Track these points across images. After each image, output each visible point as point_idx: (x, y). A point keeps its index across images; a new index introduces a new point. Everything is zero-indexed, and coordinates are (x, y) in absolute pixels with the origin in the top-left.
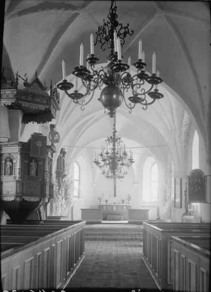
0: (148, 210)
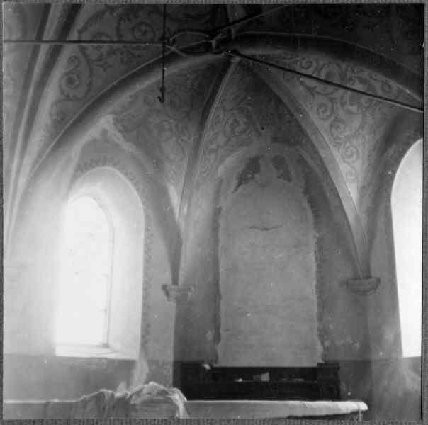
0: (420, 8)
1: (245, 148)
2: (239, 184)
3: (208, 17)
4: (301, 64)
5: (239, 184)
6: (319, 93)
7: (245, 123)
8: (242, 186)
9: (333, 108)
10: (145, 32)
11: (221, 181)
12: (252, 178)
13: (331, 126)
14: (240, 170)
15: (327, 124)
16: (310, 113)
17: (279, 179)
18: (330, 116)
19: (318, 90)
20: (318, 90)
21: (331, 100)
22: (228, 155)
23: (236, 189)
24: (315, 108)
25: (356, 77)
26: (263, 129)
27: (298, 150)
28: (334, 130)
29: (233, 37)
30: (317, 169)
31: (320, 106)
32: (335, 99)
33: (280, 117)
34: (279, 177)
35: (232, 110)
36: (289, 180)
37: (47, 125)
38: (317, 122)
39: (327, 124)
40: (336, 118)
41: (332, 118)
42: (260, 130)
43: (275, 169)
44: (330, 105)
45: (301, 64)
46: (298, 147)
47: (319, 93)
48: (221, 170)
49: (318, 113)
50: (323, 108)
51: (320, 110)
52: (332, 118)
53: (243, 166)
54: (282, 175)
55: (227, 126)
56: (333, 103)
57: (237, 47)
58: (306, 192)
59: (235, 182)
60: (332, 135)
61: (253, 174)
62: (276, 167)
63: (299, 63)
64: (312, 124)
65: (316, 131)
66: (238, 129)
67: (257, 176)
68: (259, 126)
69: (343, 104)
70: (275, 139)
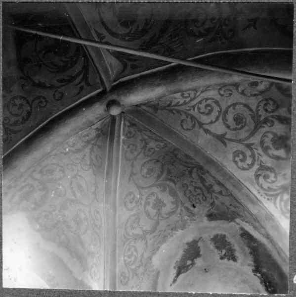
0: (289, 8)
1: (179, 232)
2: (178, 274)
3: (81, 76)
4: (199, 109)
5: (178, 274)
6: (230, 140)
7: (173, 203)
8: (182, 276)
9: (253, 156)
10: (21, 105)
11: (158, 273)
12: (193, 264)
13: (257, 176)
14: (178, 258)
15: (251, 173)
16: (225, 164)
17: (223, 261)
18: (253, 164)
19: (228, 136)
20: (228, 136)
21: (249, 146)
22: (161, 243)
23: (175, 281)
24: (231, 157)
25: (272, 117)
26: (194, 207)
27: (238, 224)
28: (261, 180)
29: (108, 89)
30: (264, 240)
31: (236, 154)
32: (253, 144)
33: (209, 189)
34: (222, 258)
35: (150, 187)
36: (234, 259)
37: (177, 262)
38: (239, 175)
39: (251, 173)
40: (268, 169)
41: (256, 167)
42: (192, 208)
43: (216, 250)
44: (248, 153)
45: (199, 109)
46: (238, 220)
47: (230, 140)
48: (156, 261)
49: (236, 162)
50: (241, 157)
51: (237, 159)
52: (256, 167)
53: (181, 253)
54: (225, 255)
55: (149, 208)
56: (251, 149)
57: (114, 97)
58: (257, 270)
59: (173, 272)
60: (262, 187)
61: (192, 260)
62: (217, 248)
63: (196, 109)
64: (230, 177)
65: (238, 185)
66: (165, 210)
67: (199, 262)
68: (188, 205)
69: (266, 149)
70: (211, 217)
